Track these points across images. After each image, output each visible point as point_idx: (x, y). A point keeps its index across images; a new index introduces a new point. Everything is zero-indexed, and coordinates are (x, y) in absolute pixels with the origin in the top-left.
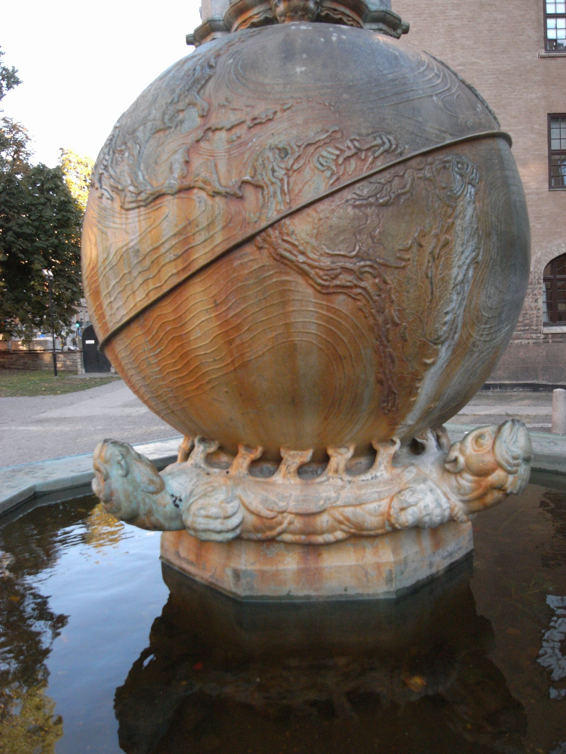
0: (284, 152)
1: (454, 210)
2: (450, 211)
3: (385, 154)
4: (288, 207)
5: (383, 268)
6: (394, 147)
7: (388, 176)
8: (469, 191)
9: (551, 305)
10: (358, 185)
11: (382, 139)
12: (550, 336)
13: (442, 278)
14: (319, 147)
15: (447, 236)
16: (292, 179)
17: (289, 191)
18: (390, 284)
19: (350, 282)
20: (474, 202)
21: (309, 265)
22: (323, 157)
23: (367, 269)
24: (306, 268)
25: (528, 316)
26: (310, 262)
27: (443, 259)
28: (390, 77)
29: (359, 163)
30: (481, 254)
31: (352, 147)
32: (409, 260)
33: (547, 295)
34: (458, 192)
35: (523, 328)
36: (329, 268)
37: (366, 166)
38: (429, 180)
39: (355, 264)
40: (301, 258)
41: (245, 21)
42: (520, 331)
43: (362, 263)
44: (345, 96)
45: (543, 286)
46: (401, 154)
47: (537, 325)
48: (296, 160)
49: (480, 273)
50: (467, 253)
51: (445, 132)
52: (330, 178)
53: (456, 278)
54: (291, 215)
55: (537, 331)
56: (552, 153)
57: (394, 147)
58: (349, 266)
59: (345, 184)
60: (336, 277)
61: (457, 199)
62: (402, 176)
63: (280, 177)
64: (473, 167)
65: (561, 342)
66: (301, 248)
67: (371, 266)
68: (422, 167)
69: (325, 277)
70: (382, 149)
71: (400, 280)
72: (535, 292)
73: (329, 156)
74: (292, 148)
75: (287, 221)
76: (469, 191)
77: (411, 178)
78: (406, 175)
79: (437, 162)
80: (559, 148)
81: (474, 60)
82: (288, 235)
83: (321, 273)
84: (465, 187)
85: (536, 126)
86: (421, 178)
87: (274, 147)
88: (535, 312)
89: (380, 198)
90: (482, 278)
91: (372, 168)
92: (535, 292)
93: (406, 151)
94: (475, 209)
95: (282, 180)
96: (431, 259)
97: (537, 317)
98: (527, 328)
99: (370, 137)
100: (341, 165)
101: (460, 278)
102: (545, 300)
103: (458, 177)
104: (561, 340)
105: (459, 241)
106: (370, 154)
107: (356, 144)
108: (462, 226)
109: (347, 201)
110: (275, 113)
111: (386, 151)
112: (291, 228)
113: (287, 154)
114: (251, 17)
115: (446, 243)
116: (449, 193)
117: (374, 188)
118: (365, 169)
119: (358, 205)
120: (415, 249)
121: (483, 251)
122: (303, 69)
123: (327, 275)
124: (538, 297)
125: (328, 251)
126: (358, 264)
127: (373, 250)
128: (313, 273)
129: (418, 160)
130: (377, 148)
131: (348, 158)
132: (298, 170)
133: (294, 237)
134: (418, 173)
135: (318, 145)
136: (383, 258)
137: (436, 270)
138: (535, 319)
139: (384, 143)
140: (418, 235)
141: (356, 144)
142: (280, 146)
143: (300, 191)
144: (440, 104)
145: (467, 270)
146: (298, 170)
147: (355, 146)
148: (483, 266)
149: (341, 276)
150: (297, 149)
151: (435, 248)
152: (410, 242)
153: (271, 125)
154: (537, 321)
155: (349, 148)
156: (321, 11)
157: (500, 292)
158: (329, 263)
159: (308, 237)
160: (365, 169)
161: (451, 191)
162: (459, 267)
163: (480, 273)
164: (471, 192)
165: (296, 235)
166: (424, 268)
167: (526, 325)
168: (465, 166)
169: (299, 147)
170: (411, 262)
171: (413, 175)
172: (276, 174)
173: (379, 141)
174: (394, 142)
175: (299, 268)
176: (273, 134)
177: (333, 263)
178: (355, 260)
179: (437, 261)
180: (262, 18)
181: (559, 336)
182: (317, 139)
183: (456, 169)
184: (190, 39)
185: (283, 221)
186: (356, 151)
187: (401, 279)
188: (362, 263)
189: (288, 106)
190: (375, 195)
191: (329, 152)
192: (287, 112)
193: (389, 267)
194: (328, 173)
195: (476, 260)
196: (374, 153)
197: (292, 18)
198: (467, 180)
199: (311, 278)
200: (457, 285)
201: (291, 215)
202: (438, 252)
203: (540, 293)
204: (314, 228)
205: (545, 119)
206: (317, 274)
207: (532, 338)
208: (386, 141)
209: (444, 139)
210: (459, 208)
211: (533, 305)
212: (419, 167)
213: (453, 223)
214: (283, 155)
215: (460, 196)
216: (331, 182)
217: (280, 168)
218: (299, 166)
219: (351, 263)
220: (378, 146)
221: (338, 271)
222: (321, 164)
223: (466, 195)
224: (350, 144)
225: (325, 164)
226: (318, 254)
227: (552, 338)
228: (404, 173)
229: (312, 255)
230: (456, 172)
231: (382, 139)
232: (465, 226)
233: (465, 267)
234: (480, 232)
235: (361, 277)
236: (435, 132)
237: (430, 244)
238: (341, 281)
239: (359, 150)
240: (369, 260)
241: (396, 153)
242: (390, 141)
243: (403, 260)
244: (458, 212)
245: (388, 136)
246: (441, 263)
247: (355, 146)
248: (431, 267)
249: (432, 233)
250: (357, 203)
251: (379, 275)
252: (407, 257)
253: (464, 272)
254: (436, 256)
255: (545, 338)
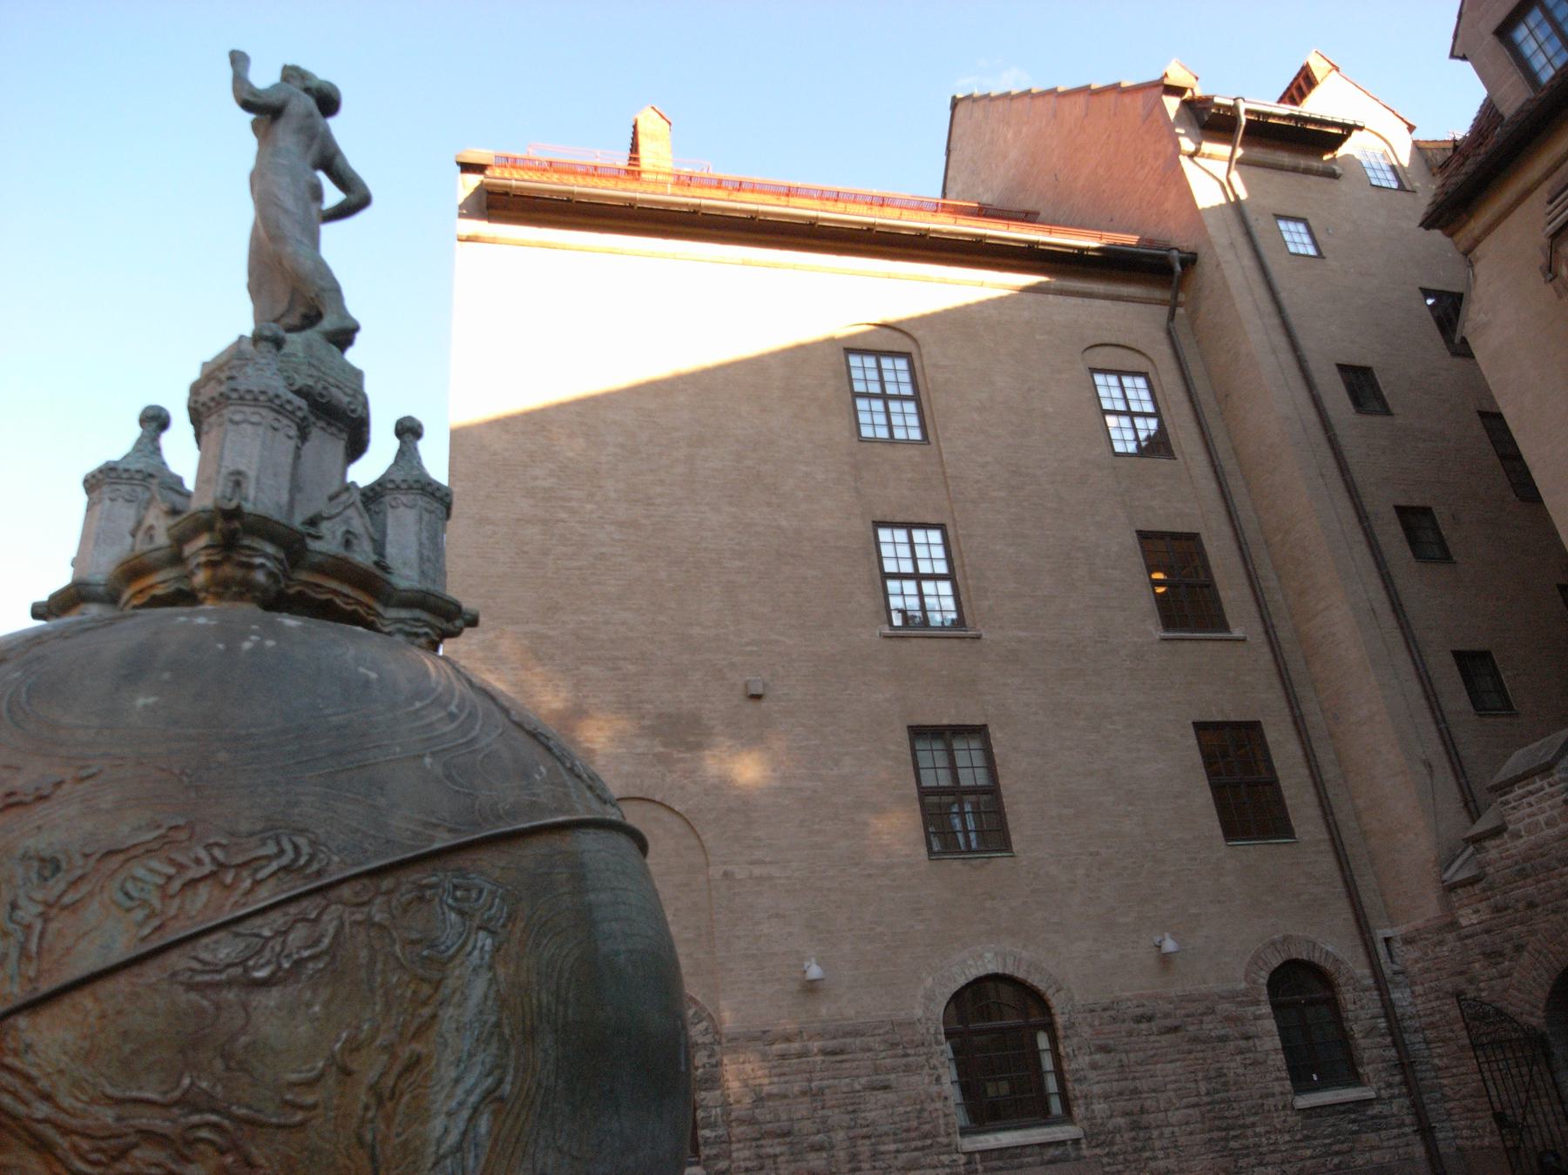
0: (50, 865)
1: (436, 989)
2: (426, 990)
3: (281, 875)
4: (29, 987)
5: (246, 1128)
6: (302, 861)
7: (281, 921)
8: (479, 944)
9: (969, 1088)
10: (205, 940)
11: (278, 843)
12: (978, 1156)
13: (405, 1144)
14: (135, 857)
15: (417, 1047)
16: (53, 926)
17: (39, 953)
18: (261, 1167)
19: (157, 1165)
20: (491, 968)
21: (56, 1126)
22: (134, 879)
23: (204, 1133)
24: (51, 1133)
25: (926, 1114)
26: (63, 1118)
27: (407, 1098)
28: (335, 720)
29: (216, 893)
30: (509, 1078)
31: (207, 860)
32: (315, 1106)
33: (958, 1066)
34: (448, 948)
35: (919, 1144)
36: (107, 1133)
37: (232, 900)
38: (381, 927)
39: (174, 1121)
40: (42, 1110)
41: (141, 591)
42: (916, 1149)
43: (196, 1118)
44: (222, 756)
45: (947, 1047)
46: (319, 874)
47: (949, 1135)
48: (74, 884)
49: (510, 1121)
50: (470, 1081)
51: (436, 826)
52: (141, 925)
53: (439, 1142)
54: (33, 1006)
55: (950, 1148)
56: (924, 792)
57: (302, 861)
58: (160, 1124)
59: (182, 934)
60: (123, 1154)
61: (444, 964)
62: (316, 920)
63: (28, 919)
64: (493, 894)
65: (1000, 1169)
66: (43, 1084)
67: (215, 1127)
68: (366, 898)
69: (95, 1156)
70: (274, 866)
71: (289, 1157)
72: (934, 1062)
73: (148, 877)
74: (70, 859)
75: (22, 1022)
76: (479, 944)
77: (335, 923)
78: (325, 918)
79: (403, 889)
80: (934, 784)
81: (774, 637)
82: (16, 1053)
83: (85, 1145)
84: (468, 938)
85: (892, 747)
86: (359, 923)
87: (32, 853)
88: (939, 1105)
89: (255, 968)
90: (516, 1132)
91: (244, 905)
92: (934, 1062)
93: (332, 868)
94: (493, 981)
95: (29, 927)
96: (373, 1101)
97: (946, 1115)
98: (929, 1142)
99: (254, 841)
100: (172, 897)
101: (453, 1139)
102: (955, 1078)
103: (453, 916)
104: (1000, 1164)
105: (449, 1056)
106: (245, 873)
107: (217, 853)
108: (458, 1022)
109: (174, 975)
110: (59, 784)
111: (285, 869)
112: (29, 1036)
113: (57, 868)
114: (151, 587)
115: (415, 1062)
116: (425, 953)
117: (242, 946)
118: (227, 908)
119: (198, 984)
120: (331, 1081)
121: (516, 1070)
122: (151, 700)
123: (99, 1150)
124: (941, 1071)
125: (109, 1091)
126: (183, 1120)
127: (225, 1087)
128: (66, 1145)
129: (358, 886)
130: (264, 862)
131: (193, 883)
132: (73, 907)
133: (30, 1057)
134: (353, 913)
135: (132, 853)
136: (249, 1107)
137: (388, 1127)
138: (941, 1121)
139: (282, 852)
140: (342, 1048)
141: (217, 853)
142: (47, 853)
143: (68, 950)
144: (439, 771)
145: (470, 1119)
146: (73, 907)
147: (214, 859)
148: (517, 1107)
149: (137, 1153)
150: (80, 862)
151: (382, 1075)
152: (320, 1064)
153: (42, 808)
154: (947, 1124)
155: (198, 862)
156: (288, 587)
157: (762, 1099)
158: (110, 1120)
159: (64, 1058)
160: (227, 908)
161: (431, 947)
162: (449, 1114)
163: (510, 1121)
164: (482, 948)
165: (35, 1053)
166: (355, 1122)
167: (925, 1137)
168: (474, 895)
169: (87, 856)
170: (320, 1111)
171: (340, 918)
172: (19, 914)
173: (271, 849)
174: (306, 849)
175: (34, 1135)
176: (39, 828)
177: (119, 1119)
178: (176, 1111)
179: (389, 1105)
180: (172, 589)
181: (995, 1154)
182: (130, 842)
183: (450, 901)
184: (40, 611)
185: (11, 1021)
186: (214, 868)
187: (293, 1154)
188: (196, 1118)
189: (93, 770)
190: (243, 962)
191: (151, 870)
192: (87, 784)
193: (263, 1125)
194: (139, 914)
195: (497, 1094)
196: (256, 871)
197: (219, 597)
198: (477, 922)
199: (59, 1159)
200: (444, 1157)
201: (33, 1006)
202: (391, 1083)
203: (943, 1064)
204: (85, 1038)
205: (905, 735)
206: (75, 1148)
207: (944, 1166)
208: (288, 847)
209: (432, 839)
210: (451, 983)
211: (934, 1089)
212: (360, 900)
213: (434, 1016)
214: (47, 873)
215: (452, 958)
216: (146, 931)
217: (31, 899)
218: (77, 896)
219: (165, 1120)
220: (269, 858)
221: (132, 1139)
222: (127, 894)
223: (470, 954)
224: (203, 854)
225: (135, 894)
226: (84, 1098)
227: (982, 1161)
228: (320, 915)
229: (67, 1102)
230: (449, 906)
231: (278, 843)
232: (466, 1019)
233: (465, 1114)
234: (507, 1031)
235: (186, 1152)
236: (411, 826)
237: (370, 1067)
238: (133, 1164)
239: (222, 866)
240: (213, 1111)
241: (308, 871)
242: (296, 848)
243: (301, 1107)
244: (448, 991)
245: (295, 839)
246: (401, 1108)
247: (214, 859)
248: (372, 1121)
249: (378, 1042)
250: (199, 978)
251: (235, 1147)
252: (310, 1099)
253: (462, 1125)
254: (387, 1094)
255: (968, 1163)
